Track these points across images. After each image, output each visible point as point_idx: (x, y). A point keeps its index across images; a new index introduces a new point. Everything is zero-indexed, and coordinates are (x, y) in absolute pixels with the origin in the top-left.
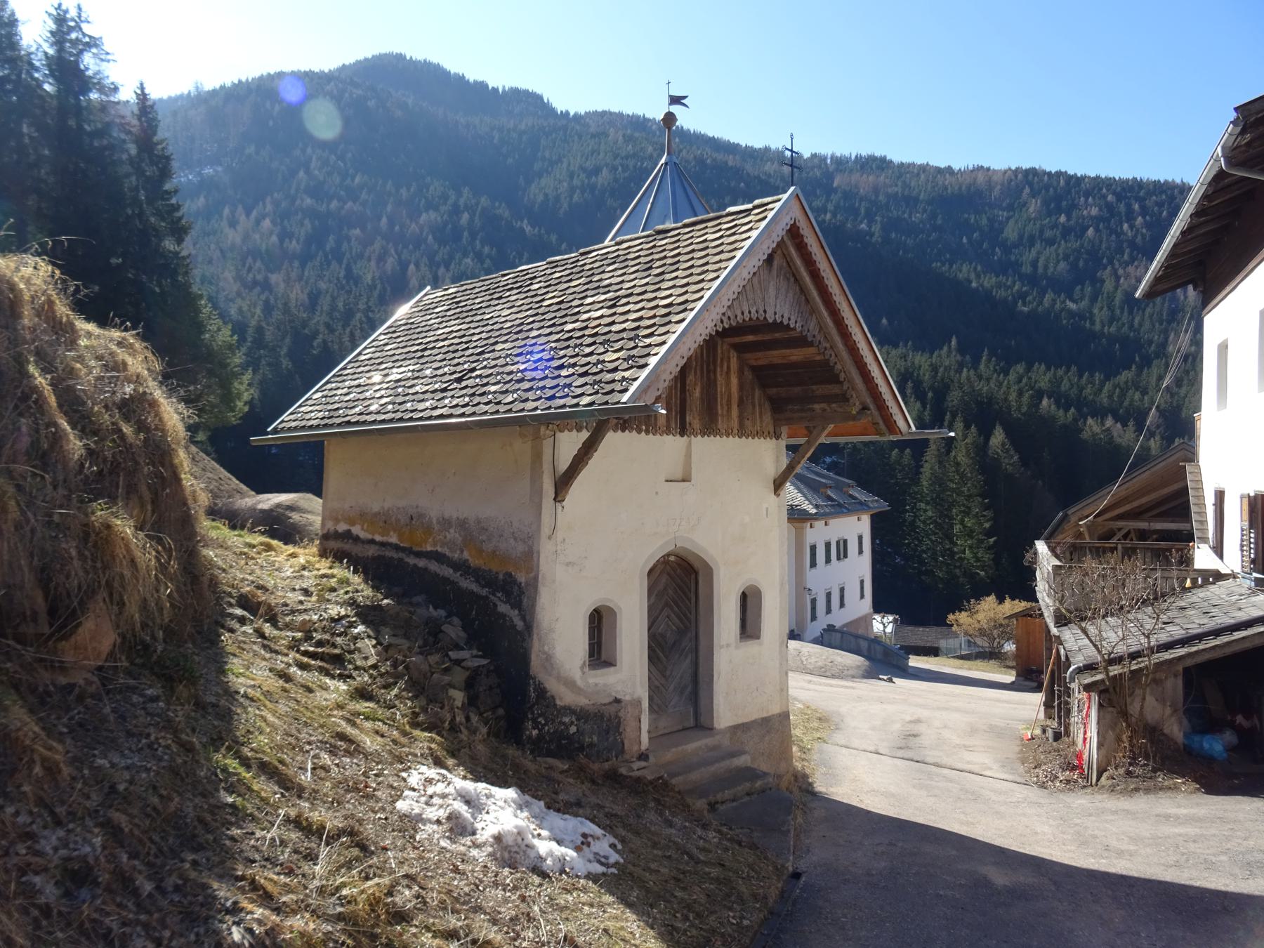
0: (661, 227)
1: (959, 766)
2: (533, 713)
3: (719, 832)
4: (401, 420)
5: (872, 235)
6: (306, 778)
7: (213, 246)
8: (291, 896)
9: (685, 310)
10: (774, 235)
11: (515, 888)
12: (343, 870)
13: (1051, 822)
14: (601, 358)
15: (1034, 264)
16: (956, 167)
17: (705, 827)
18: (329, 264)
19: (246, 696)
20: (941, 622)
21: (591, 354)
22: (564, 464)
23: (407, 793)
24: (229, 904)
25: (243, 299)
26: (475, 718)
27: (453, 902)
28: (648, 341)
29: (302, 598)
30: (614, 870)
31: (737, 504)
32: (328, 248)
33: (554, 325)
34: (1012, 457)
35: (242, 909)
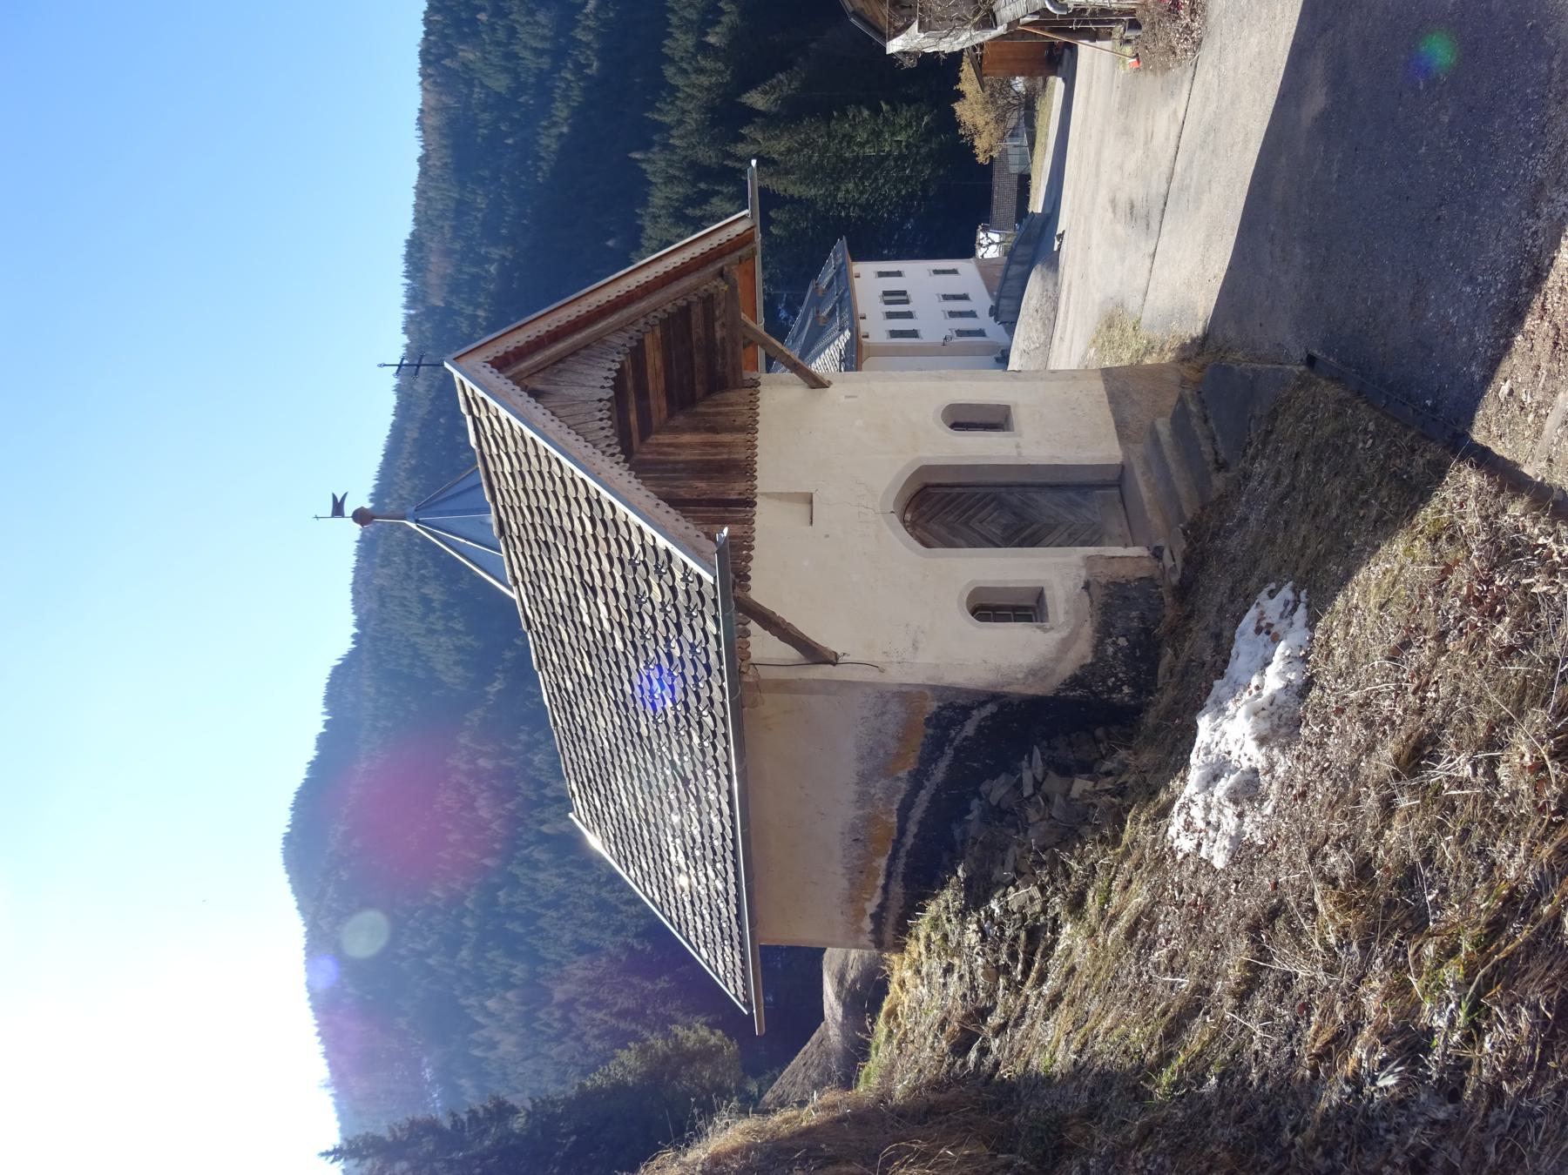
0: (495, 529)
1: (1172, 151)
2: (1102, 692)
3: (1254, 458)
4: (734, 853)
5: (504, 258)
6: (1186, 983)
7: (520, 1070)
8: (1337, 1009)
9: (598, 501)
10: (505, 388)
11: (1326, 720)
12: (1304, 941)
13: (1245, 33)
14: (658, 606)
15: (539, 53)
16: (419, 152)
17: (1247, 477)
18: (542, 930)
19: (1080, 1053)
20: (987, 171)
21: (653, 619)
22: (789, 653)
23: (1203, 854)
24: (1348, 1089)
25: (584, 1034)
26: (1108, 765)
27: (1345, 800)
28: (637, 548)
29: (956, 976)
30: (1303, 594)
31: (841, 431)
32: (521, 930)
33: (617, 664)
34: (780, 81)
35: (1356, 1073)
